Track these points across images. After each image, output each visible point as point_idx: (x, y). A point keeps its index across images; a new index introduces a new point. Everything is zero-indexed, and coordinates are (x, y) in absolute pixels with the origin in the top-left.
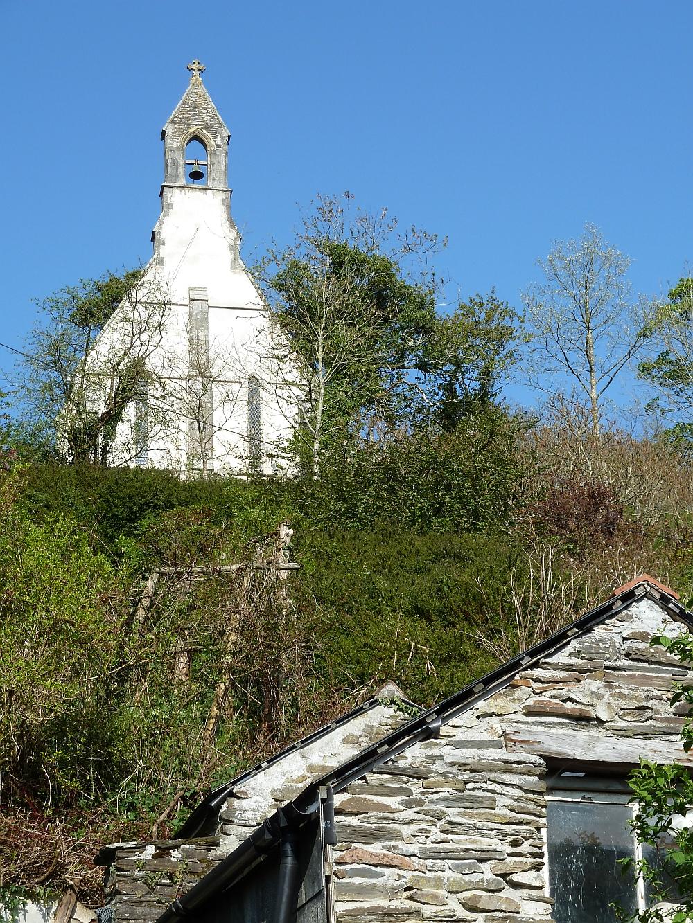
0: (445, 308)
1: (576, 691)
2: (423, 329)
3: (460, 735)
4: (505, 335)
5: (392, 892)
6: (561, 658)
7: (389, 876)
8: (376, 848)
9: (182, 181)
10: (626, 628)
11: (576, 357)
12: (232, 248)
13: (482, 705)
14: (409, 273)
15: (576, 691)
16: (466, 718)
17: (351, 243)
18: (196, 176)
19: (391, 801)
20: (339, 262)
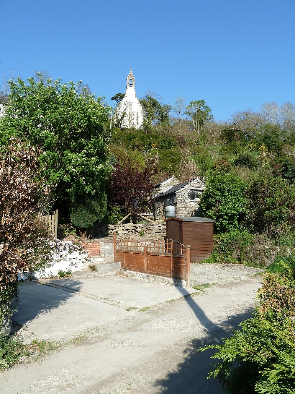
0: (162, 105)
1: (193, 184)
2: (160, 109)
3: (185, 188)
4: (169, 109)
5: (181, 198)
6: (192, 182)
7: (181, 197)
8: (180, 195)
9: (129, 85)
10: (196, 180)
11: (178, 113)
12: (135, 95)
13: (187, 185)
14: (158, 101)
15: (193, 184)
16: (185, 186)
17: (151, 97)
18: (131, 85)
19: (181, 192)
20: (150, 99)
